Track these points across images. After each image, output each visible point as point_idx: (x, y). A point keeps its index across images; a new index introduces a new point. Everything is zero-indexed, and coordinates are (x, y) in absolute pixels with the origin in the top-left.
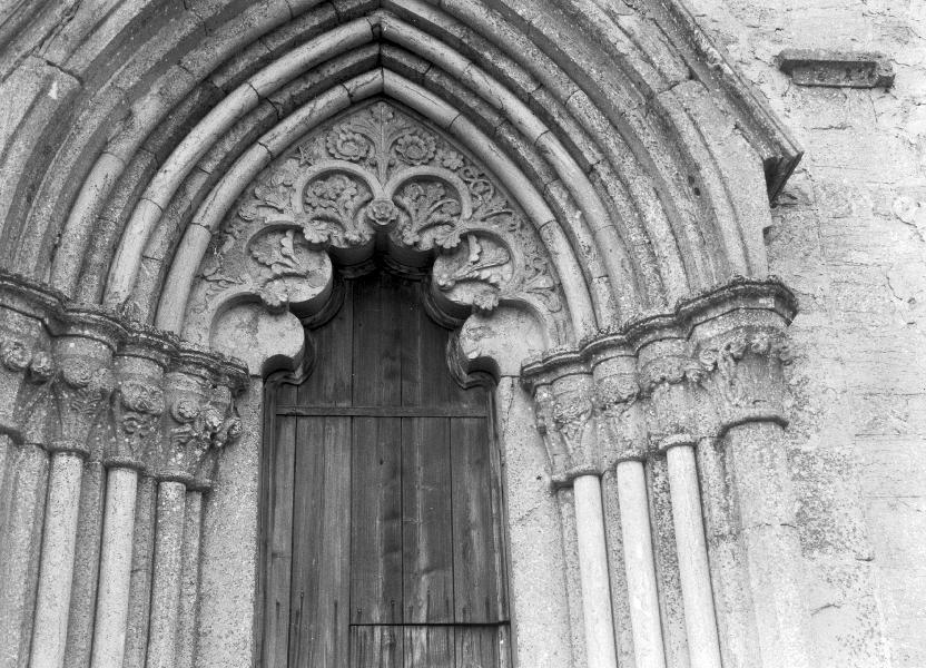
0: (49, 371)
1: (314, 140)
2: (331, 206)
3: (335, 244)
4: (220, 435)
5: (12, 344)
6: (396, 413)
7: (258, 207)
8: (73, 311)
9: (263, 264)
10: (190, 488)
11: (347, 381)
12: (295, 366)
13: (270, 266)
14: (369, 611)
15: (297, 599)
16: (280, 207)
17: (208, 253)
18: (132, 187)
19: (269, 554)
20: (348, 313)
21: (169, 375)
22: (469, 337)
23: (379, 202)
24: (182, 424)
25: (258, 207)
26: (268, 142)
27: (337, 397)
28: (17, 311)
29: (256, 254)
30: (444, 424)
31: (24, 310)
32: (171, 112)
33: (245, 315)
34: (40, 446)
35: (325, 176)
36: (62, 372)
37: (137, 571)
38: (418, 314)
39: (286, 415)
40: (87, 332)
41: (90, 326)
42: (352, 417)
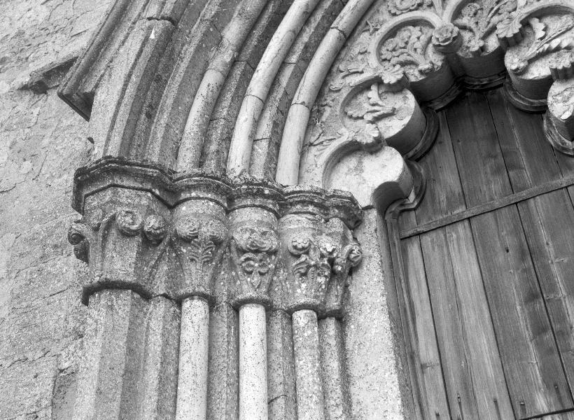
0: (159, 228)
1: (378, 11)
2: (402, 53)
3: (413, 79)
4: (338, 260)
5: (123, 213)
6: (510, 201)
7: (344, 77)
8: (178, 179)
9: (358, 118)
10: (322, 315)
11: (457, 190)
12: (405, 192)
13: (362, 118)
14: (533, 403)
15: (456, 407)
16: (360, 70)
17: (310, 125)
18: (233, 90)
19: (418, 366)
20: (445, 136)
21: (282, 220)
22: (557, 101)
23: (440, 29)
24: (298, 256)
25: (344, 77)
26: (338, 23)
27: (451, 206)
28: (127, 188)
29: (350, 113)
30: (562, 195)
31: (132, 185)
32: (253, 26)
33: (352, 162)
34: (165, 296)
35: (393, 33)
36: (176, 230)
37: (272, 401)
38: (509, 112)
39: (410, 237)
40: (193, 194)
41: (194, 187)
42: (469, 219)
